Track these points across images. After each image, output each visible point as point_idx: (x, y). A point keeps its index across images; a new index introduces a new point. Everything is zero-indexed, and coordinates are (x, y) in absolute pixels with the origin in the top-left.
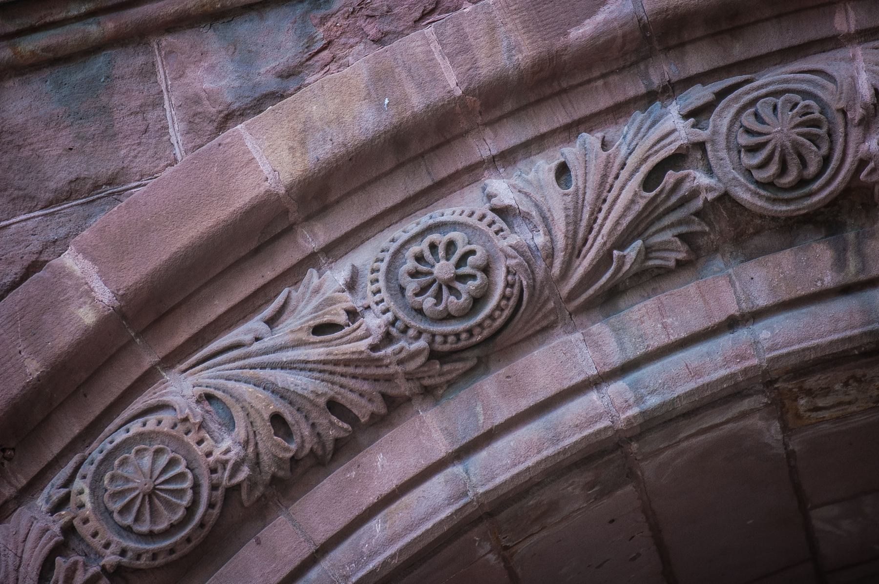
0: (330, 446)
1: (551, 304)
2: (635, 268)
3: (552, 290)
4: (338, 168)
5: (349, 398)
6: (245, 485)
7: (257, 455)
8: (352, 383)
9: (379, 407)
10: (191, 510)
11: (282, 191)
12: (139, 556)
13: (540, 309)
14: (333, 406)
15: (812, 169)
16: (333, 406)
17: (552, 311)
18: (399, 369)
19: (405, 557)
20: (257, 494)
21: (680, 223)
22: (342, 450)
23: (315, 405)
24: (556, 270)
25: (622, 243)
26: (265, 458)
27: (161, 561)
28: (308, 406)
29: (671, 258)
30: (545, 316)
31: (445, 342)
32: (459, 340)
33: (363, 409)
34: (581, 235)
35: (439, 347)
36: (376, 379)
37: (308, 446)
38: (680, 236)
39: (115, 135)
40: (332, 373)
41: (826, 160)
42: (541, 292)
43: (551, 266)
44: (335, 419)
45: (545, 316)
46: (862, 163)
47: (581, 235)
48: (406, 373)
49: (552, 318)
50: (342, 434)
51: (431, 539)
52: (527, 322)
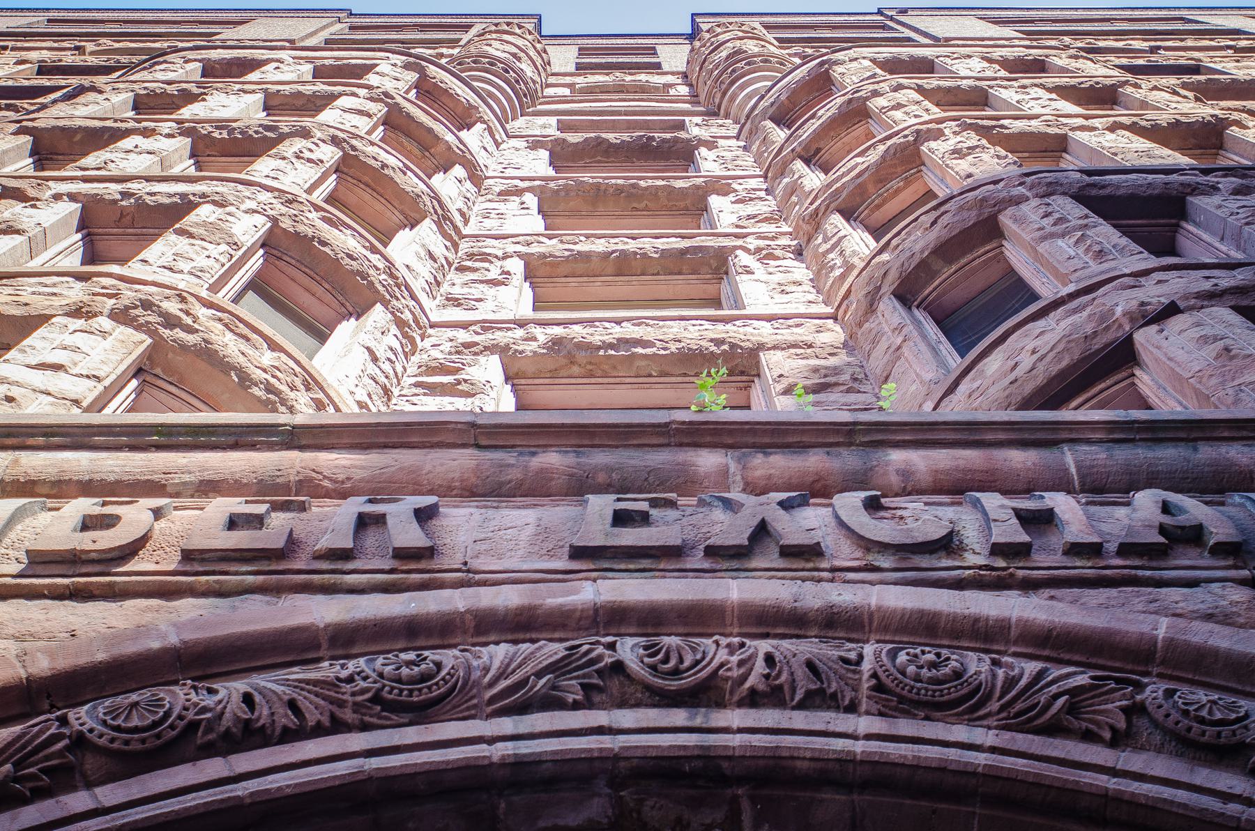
0: (278, 731)
1: (475, 701)
2: (544, 691)
3: (479, 692)
4: (365, 627)
5: (304, 704)
6: (204, 723)
7: (222, 713)
8: (312, 697)
9: (326, 720)
10: (155, 724)
11: (322, 625)
12: (101, 736)
13: (466, 702)
14: (292, 705)
15: (687, 664)
16: (292, 705)
17: (475, 706)
18: (350, 698)
19: (297, 791)
20: (210, 737)
21: (584, 676)
22: (289, 736)
23: (281, 699)
24: (487, 679)
25: (539, 674)
26: (227, 715)
27: (115, 745)
28: (275, 699)
29: (570, 698)
30: (468, 709)
31: (390, 693)
32: (400, 695)
33: (312, 717)
34: (512, 667)
35: (385, 694)
36: (332, 701)
37: (262, 722)
38: (581, 684)
39: (204, 340)
40: (302, 689)
41: (697, 662)
42: (471, 689)
43: (485, 675)
44: (290, 713)
45: (468, 709)
46: (722, 665)
47: (512, 667)
48: (355, 704)
49: (473, 712)
50: (291, 725)
51: (323, 786)
52: (454, 707)
